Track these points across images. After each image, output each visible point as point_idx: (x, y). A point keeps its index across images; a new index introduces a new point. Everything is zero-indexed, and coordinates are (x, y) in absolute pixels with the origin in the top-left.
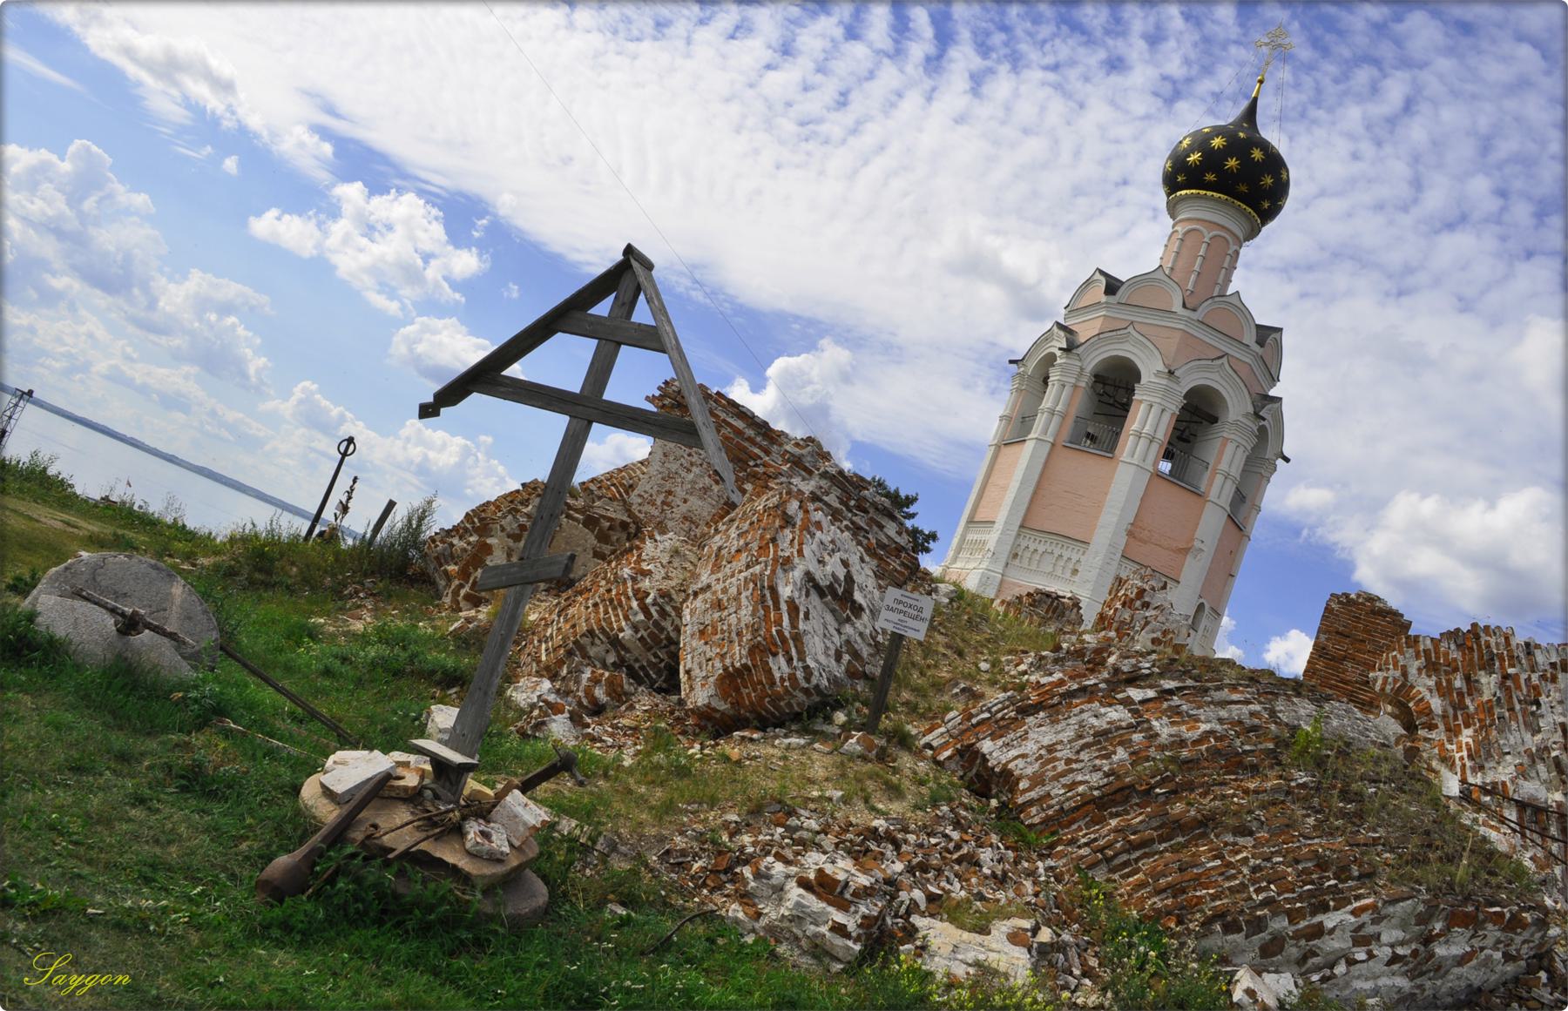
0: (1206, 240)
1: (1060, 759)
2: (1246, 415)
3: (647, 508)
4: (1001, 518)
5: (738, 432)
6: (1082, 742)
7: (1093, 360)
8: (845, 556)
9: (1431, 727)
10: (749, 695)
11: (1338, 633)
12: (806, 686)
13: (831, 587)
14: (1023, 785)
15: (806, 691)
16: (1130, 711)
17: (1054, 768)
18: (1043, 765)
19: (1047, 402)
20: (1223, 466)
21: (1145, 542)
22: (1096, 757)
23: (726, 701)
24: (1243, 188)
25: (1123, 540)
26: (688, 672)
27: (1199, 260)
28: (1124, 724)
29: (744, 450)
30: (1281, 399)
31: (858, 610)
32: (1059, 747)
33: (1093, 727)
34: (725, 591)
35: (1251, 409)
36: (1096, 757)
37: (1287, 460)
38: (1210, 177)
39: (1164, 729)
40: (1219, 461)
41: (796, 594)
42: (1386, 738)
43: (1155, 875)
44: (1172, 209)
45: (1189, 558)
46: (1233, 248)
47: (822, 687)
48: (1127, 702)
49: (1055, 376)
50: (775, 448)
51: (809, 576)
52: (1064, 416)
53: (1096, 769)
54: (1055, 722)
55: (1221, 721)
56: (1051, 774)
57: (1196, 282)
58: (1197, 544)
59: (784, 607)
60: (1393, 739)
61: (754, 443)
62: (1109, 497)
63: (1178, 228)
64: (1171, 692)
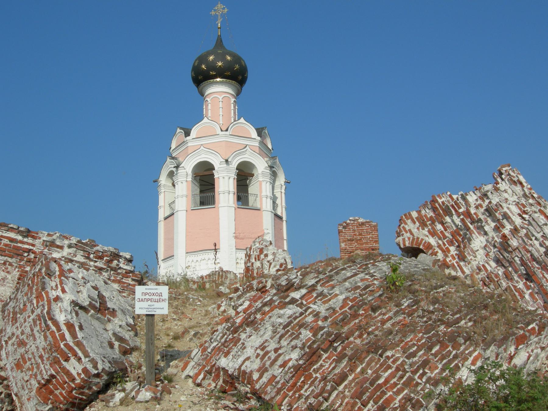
0: (221, 100)
1: (271, 351)
6: (278, 336)
8: (94, 285)
10: (61, 394)
11: (348, 240)
12: (96, 372)
13: (91, 304)
14: (255, 376)
15: (98, 375)
16: (297, 306)
17: (269, 358)
18: (262, 359)
20: (264, 193)
21: (243, 239)
22: (291, 341)
23: (47, 404)
25: (233, 241)
26: (16, 395)
28: (297, 315)
29: (19, 248)
31: (113, 313)
32: (266, 344)
33: (280, 324)
34: (23, 333)
36: (291, 341)
39: (321, 308)
40: (261, 191)
41: (69, 317)
42: (427, 265)
47: (107, 369)
48: (293, 301)
51: (75, 303)
53: (294, 348)
54: (256, 329)
56: (268, 363)
58: (266, 231)
59: (64, 328)
60: (431, 265)
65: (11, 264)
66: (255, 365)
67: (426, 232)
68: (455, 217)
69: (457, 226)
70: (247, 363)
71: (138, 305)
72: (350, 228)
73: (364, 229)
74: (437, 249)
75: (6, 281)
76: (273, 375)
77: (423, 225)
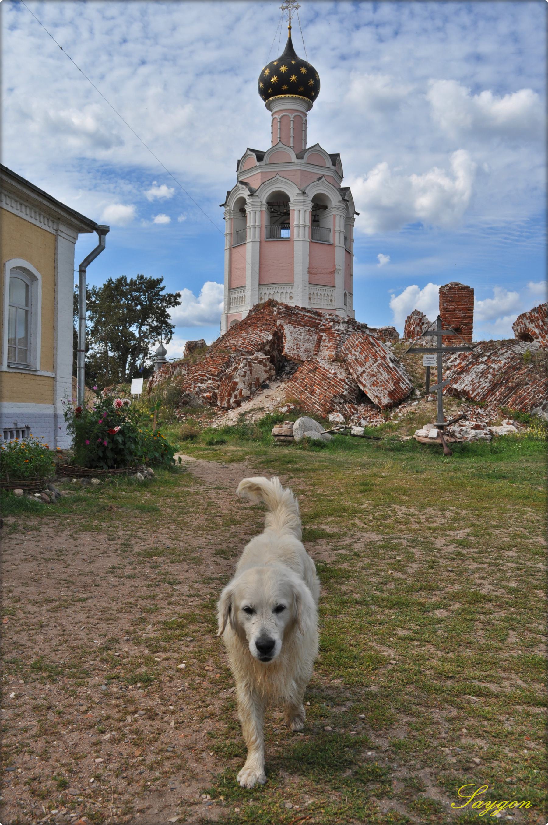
2: (340, 202)
3: (292, 352)
4: (248, 283)
5: (310, 317)
7: (264, 196)
9: (537, 338)
14: (471, 392)
19: (250, 221)
20: (337, 228)
21: (316, 274)
24: (302, 89)
25: (307, 277)
27: (292, 130)
30: (349, 188)
35: (341, 198)
37: (358, 214)
38: (286, 87)
43: (514, 401)
44: (268, 107)
45: (336, 275)
46: (304, 119)
48: (482, 362)
49: (248, 209)
50: (322, 318)
52: (261, 227)
53: (486, 382)
54: (468, 374)
55: (505, 359)
57: (293, 141)
58: (337, 267)
61: (316, 319)
62: (295, 259)
63: (275, 116)
64: (489, 356)
65: (312, 331)
66: (471, 388)
67: (533, 325)
71: (424, 362)
74: (539, 336)
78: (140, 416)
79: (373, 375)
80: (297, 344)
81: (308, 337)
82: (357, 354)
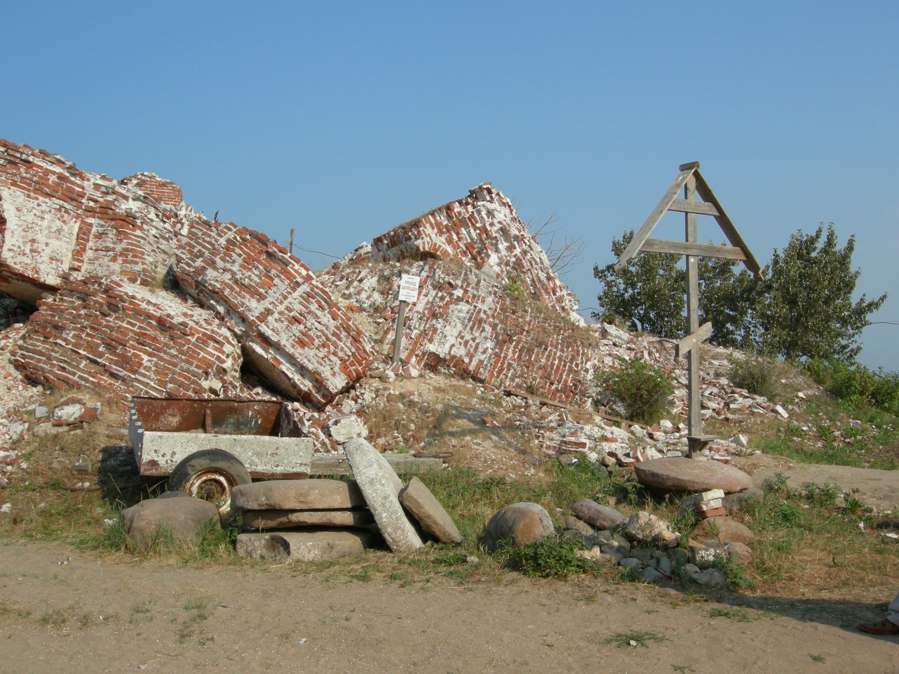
3: (20, 259)
14: (466, 360)
56: (472, 350)
65: (67, 211)
68: (472, 231)
69: (472, 239)
70: (454, 349)
72: (147, 188)
73: (165, 192)
75: (62, 233)
76: (480, 360)
77: (441, 233)
78: (840, 308)
79: (296, 320)
80: (33, 241)
81: (59, 224)
82: (235, 268)
